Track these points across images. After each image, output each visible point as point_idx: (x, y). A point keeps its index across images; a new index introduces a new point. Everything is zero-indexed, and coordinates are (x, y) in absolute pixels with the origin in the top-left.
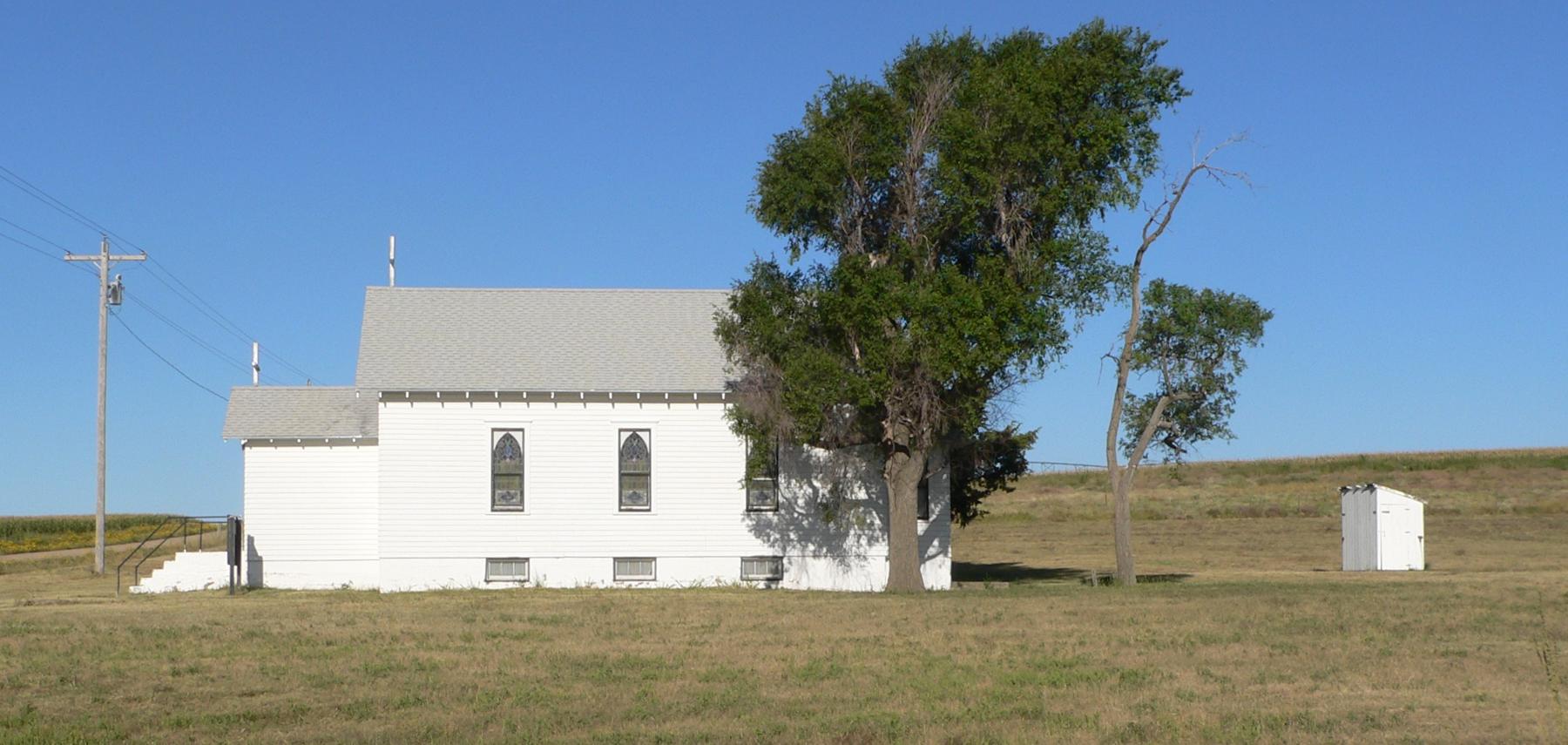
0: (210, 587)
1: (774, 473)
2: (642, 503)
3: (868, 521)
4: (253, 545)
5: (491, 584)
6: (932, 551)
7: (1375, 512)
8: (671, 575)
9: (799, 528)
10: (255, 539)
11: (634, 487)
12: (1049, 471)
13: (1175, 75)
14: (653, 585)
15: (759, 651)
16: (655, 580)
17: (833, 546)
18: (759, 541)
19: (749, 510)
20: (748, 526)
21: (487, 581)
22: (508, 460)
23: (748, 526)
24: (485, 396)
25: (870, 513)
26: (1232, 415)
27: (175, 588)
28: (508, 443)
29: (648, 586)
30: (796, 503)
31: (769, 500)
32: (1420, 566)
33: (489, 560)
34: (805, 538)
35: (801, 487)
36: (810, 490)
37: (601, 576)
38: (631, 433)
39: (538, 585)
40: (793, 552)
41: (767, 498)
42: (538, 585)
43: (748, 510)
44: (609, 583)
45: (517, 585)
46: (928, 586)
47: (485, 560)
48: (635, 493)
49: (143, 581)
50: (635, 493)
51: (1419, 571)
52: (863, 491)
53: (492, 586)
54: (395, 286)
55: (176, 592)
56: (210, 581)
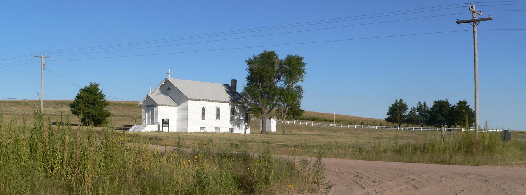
1: (233, 115)
6: (248, 127)
7: (271, 123)
8: (222, 131)
12: (4, 100)
13: (302, 97)
14: (219, 132)
15: (429, 149)
16: (219, 131)
17: (239, 126)
19: (230, 120)
21: (201, 131)
24: (216, 101)
32: (275, 131)
33: (201, 128)
34: (236, 125)
37: (213, 131)
39: (207, 132)
40: (235, 127)
42: (207, 132)
44: (215, 132)
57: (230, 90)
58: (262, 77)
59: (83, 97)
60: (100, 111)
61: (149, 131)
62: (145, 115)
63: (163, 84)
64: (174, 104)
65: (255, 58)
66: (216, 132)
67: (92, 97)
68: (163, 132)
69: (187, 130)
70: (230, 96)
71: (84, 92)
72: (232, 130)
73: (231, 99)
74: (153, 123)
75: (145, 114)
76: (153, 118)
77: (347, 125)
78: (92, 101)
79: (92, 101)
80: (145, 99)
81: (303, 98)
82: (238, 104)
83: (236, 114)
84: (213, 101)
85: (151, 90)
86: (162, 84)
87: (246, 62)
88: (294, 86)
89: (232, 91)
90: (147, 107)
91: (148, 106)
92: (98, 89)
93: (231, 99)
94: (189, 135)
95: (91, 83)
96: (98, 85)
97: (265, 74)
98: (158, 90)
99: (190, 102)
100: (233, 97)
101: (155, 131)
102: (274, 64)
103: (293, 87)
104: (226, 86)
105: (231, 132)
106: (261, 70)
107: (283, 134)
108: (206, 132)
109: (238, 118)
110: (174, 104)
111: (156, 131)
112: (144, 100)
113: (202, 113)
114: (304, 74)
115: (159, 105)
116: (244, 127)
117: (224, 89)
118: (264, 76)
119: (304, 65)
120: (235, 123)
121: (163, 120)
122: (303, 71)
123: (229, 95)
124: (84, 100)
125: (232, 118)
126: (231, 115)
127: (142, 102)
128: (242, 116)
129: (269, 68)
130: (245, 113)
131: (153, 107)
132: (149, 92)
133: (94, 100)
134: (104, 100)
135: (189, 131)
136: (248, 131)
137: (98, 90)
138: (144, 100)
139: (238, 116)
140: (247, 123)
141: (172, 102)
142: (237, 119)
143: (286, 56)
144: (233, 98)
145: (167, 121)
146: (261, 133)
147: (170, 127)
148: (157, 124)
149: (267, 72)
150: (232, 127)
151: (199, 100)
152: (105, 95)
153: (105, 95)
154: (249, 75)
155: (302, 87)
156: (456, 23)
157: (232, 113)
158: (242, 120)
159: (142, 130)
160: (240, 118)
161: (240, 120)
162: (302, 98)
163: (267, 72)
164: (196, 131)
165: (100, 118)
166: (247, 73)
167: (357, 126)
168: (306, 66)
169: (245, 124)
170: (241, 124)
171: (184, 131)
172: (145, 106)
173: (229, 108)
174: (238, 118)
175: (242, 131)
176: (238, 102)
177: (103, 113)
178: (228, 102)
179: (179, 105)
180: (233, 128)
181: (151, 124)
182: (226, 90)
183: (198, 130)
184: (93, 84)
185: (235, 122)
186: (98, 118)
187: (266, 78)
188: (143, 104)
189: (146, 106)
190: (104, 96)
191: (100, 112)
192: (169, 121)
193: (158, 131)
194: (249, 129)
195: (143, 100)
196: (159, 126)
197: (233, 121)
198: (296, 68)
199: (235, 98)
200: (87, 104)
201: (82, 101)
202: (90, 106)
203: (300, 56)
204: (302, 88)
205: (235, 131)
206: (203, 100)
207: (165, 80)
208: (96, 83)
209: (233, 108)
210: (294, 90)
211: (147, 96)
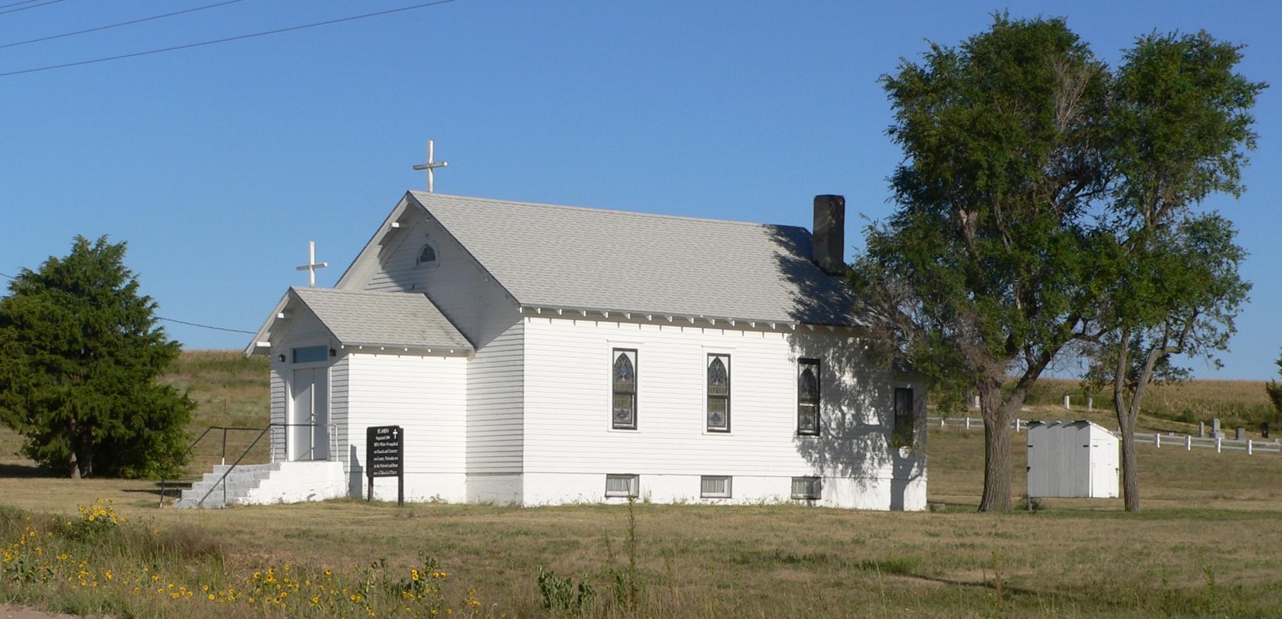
0: (312, 499)
1: (817, 401)
2: (720, 424)
3: (879, 444)
4: (355, 453)
5: (610, 499)
6: (914, 471)
7: (1087, 446)
8: (745, 492)
9: (832, 449)
10: (357, 448)
11: (716, 409)
14: (729, 502)
17: (854, 465)
18: (804, 460)
20: (797, 446)
21: (607, 497)
22: (623, 379)
23: (797, 446)
24: (702, 323)
25: (880, 436)
26: (1221, 368)
27: (281, 499)
28: (623, 363)
29: (726, 503)
30: (830, 425)
31: (810, 425)
33: (610, 476)
34: (835, 459)
35: (833, 411)
36: (840, 415)
37: (691, 493)
38: (715, 357)
40: (828, 472)
41: (809, 422)
42: (646, 501)
43: (799, 433)
44: (698, 500)
45: (625, 501)
46: (526, 506)
47: (700, 477)
48: (716, 414)
49: (252, 492)
50: (716, 414)
51: (332, 503)
52: (876, 418)
53: (611, 501)
54: (434, 192)
55: (281, 504)
56: (312, 493)
57: (810, 256)
58: (969, 171)
59: (21, 317)
60: (121, 393)
61: (291, 498)
62: (286, 408)
63: (396, 225)
64: (451, 344)
65: (941, 60)
66: (709, 502)
67: (76, 316)
69: (519, 493)
70: (803, 291)
71: (38, 291)
72: (812, 487)
73: (801, 308)
74: (322, 455)
75: (286, 402)
76: (321, 425)
77: (1152, 435)
78: (76, 340)
79: (73, 341)
80: (281, 316)
81: (1249, 294)
82: (850, 340)
83: (838, 395)
84: (681, 321)
85: (313, 263)
87: (889, 87)
88: (1178, 217)
89: (816, 263)
90: (295, 361)
91: (297, 355)
92: (115, 278)
93: (801, 308)
94: (243, 513)
95: (80, 238)
96: (118, 250)
97: (985, 149)
98: (371, 264)
99: (534, 328)
100: (819, 298)
101: (327, 501)
102: (1048, 92)
103: (1174, 228)
104: (788, 234)
105: (804, 502)
106: (961, 126)
107: (1127, 509)
108: (640, 501)
109: (848, 417)
110: (451, 344)
111: (336, 500)
112: (277, 319)
114: (1240, 147)
115: (353, 348)
116: (886, 472)
117: (768, 251)
118: (978, 165)
119: (1244, 93)
121: (372, 433)
122: (1239, 130)
123: (795, 288)
124: (31, 334)
125: (809, 424)
126: (800, 400)
127: (268, 335)
128: (872, 404)
129: (1019, 120)
130: (897, 390)
131: (324, 358)
132: (302, 272)
133: (86, 335)
134: (150, 331)
135: (531, 498)
136: (916, 497)
137: (120, 279)
138: (277, 319)
139: (848, 405)
140: (909, 444)
141: (439, 330)
142: (841, 424)
143: (1131, 46)
144: (814, 302)
145: (391, 441)
146: (982, 508)
147: (405, 476)
148: (342, 458)
149: (997, 138)
150: (808, 470)
151: (595, 315)
152: (154, 306)
153: (154, 306)
154: (909, 163)
155: (1230, 222)
157: (810, 392)
158: (873, 428)
160: (858, 417)
161: (861, 429)
162: (1243, 296)
163: (997, 138)
165: (122, 430)
166: (897, 157)
167: (1258, 446)
168: (1261, 98)
169: (894, 448)
170: (868, 455)
171: (503, 501)
172: (283, 357)
173: (792, 360)
174: (848, 417)
175: (877, 497)
176: (842, 327)
177: (137, 403)
178: (782, 328)
179: (476, 348)
181: (316, 459)
182: (783, 261)
183: (593, 491)
184: (90, 248)
185: (829, 444)
186: (109, 434)
187: (992, 175)
188: (277, 341)
189: (289, 356)
190: (149, 311)
191: (123, 400)
193: (345, 500)
194: (924, 484)
195: (270, 322)
196: (355, 472)
197: (815, 439)
198: (1184, 109)
199: (831, 305)
200: (47, 357)
201: (22, 338)
202: (68, 364)
203: (1219, 37)
204: (1228, 236)
205: (829, 493)
206: (617, 317)
207: (404, 204)
208: (112, 241)
209: (817, 362)
210: (1181, 243)
211: (287, 298)
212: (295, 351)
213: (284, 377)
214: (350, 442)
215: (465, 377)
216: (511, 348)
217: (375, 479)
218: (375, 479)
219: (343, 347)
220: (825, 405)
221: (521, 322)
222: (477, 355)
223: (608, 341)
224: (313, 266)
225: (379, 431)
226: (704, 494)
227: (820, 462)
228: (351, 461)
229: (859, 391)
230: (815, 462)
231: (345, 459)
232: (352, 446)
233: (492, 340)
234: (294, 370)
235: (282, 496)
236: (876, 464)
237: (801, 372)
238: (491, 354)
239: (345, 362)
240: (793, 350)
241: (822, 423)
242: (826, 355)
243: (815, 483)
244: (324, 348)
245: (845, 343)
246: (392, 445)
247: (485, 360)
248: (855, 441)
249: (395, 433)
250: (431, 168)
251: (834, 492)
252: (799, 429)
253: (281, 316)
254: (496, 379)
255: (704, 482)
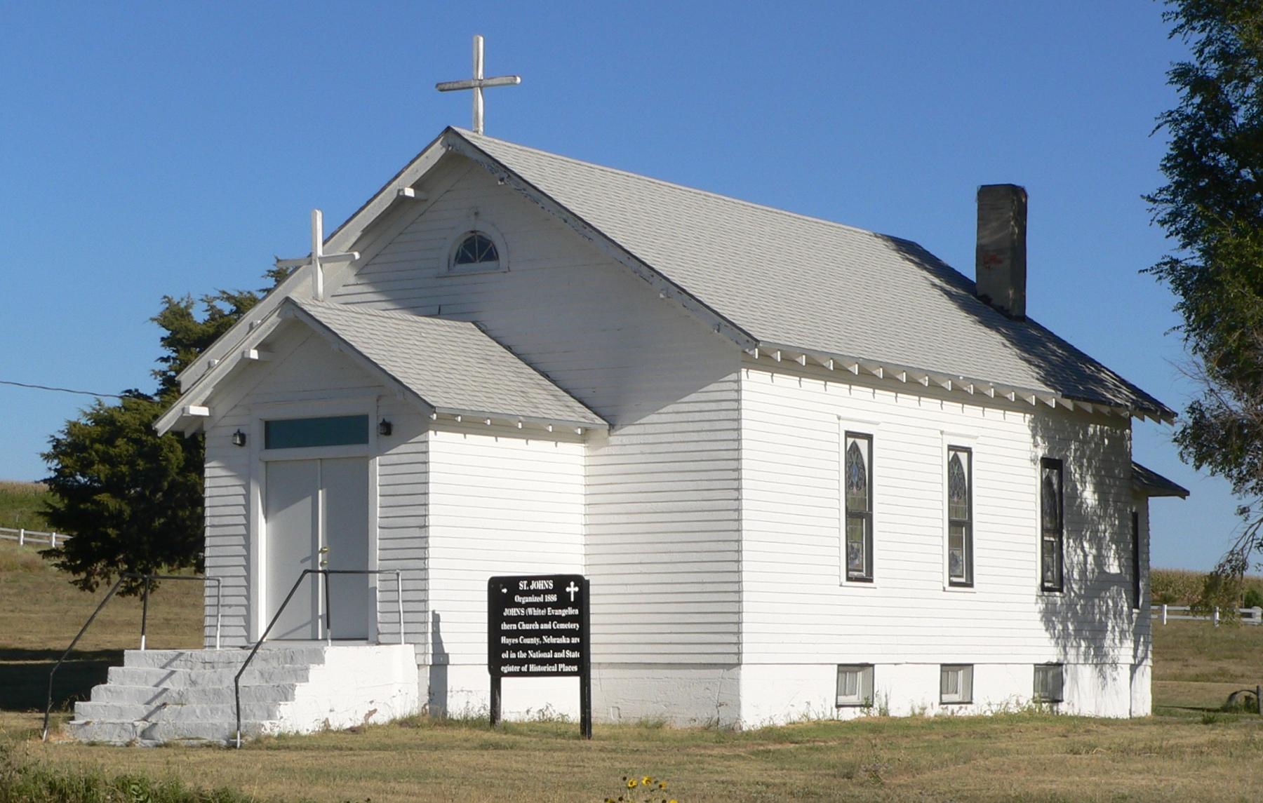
0: (371, 721)
2: (958, 573)
39: (884, 712)
43: (1043, 589)
49: (284, 709)
68: (508, 728)
75: (249, 525)
80: (254, 355)
86: (401, 200)
90: (268, 445)
101: (393, 722)
113: (969, 525)
120: (1075, 613)
145: (563, 602)
147: (594, 673)
148: (412, 637)
150: (1050, 653)
156: (164, 321)
159: (270, 716)
160: (1100, 560)
161: (1103, 581)
164: (802, 709)
167: (31, 536)
174: (1090, 559)
179: (612, 426)
180: (1059, 665)
188: (222, 409)
189: (256, 436)
192: (582, 600)
194: (1149, 670)
207: (437, 152)
212: (269, 426)
213: (246, 478)
214: (432, 606)
215: (582, 480)
216: (706, 426)
217: (504, 680)
218: (504, 680)
219: (435, 416)
220: (1068, 538)
221: (733, 376)
222: (614, 439)
223: (839, 418)
224: (320, 258)
225: (523, 585)
226: (946, 698)
227: (1063, 638)
228: (433, 644)
229: (1099, 517)
230: (1058, 638)
231: (420, 639)
232: (433, 612)
233: (654, 410)
234: (267, 462)
235: (327, 715)
236: (1117, 641)
237: (1044, 477)
238: (650, 439)
239: (421, 447)
240: (1036, 446)
241: (1065, 571)
242: (1068, 454)
243: (1050, 674)
244: (362, 420)
245: (1086, 433)
246: (563, 613)
247: (637, 449)
248: (1097, 601)
249: (572, 589)
250: (481, 88)
251: (1076, 689)
252: (1043, 581)
253: (254, 355)
254: (664, 486)
255: (840, 675)
